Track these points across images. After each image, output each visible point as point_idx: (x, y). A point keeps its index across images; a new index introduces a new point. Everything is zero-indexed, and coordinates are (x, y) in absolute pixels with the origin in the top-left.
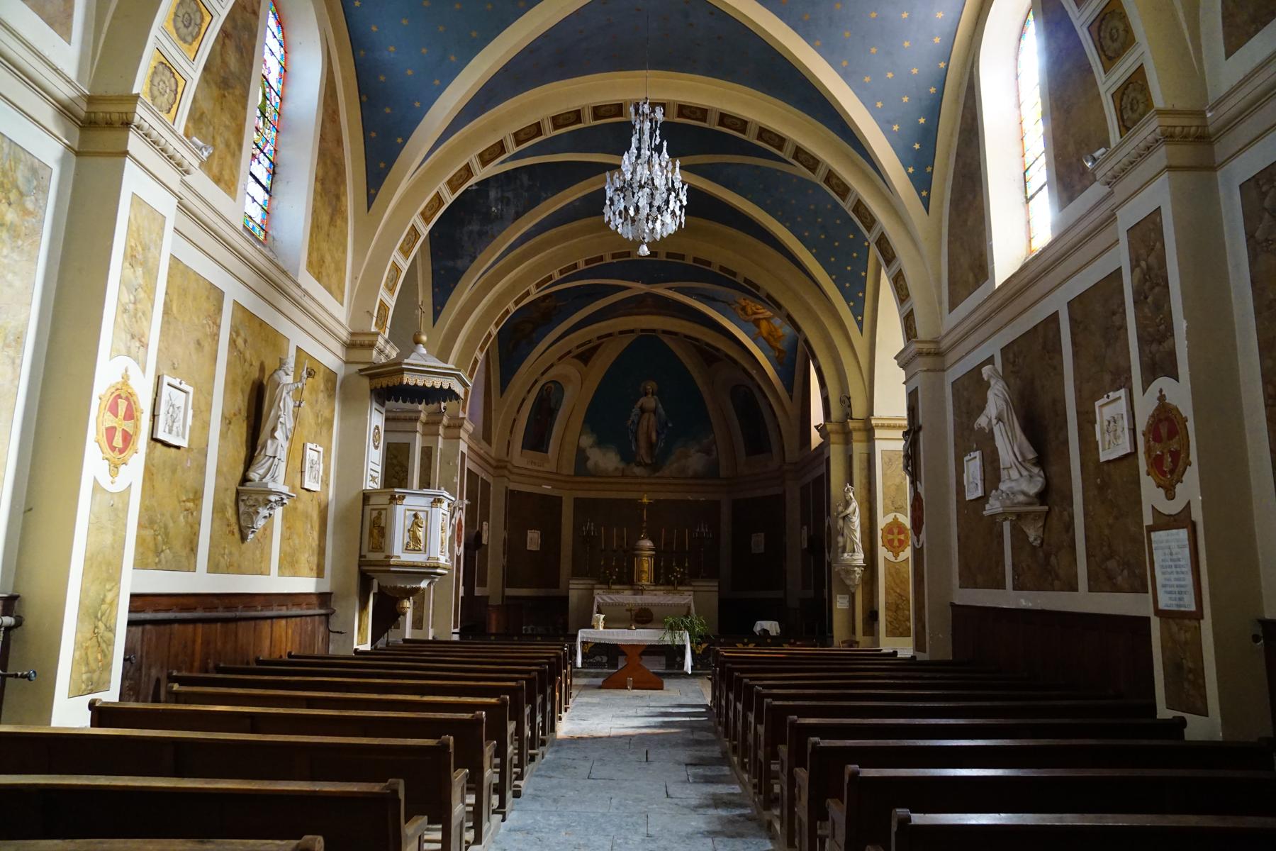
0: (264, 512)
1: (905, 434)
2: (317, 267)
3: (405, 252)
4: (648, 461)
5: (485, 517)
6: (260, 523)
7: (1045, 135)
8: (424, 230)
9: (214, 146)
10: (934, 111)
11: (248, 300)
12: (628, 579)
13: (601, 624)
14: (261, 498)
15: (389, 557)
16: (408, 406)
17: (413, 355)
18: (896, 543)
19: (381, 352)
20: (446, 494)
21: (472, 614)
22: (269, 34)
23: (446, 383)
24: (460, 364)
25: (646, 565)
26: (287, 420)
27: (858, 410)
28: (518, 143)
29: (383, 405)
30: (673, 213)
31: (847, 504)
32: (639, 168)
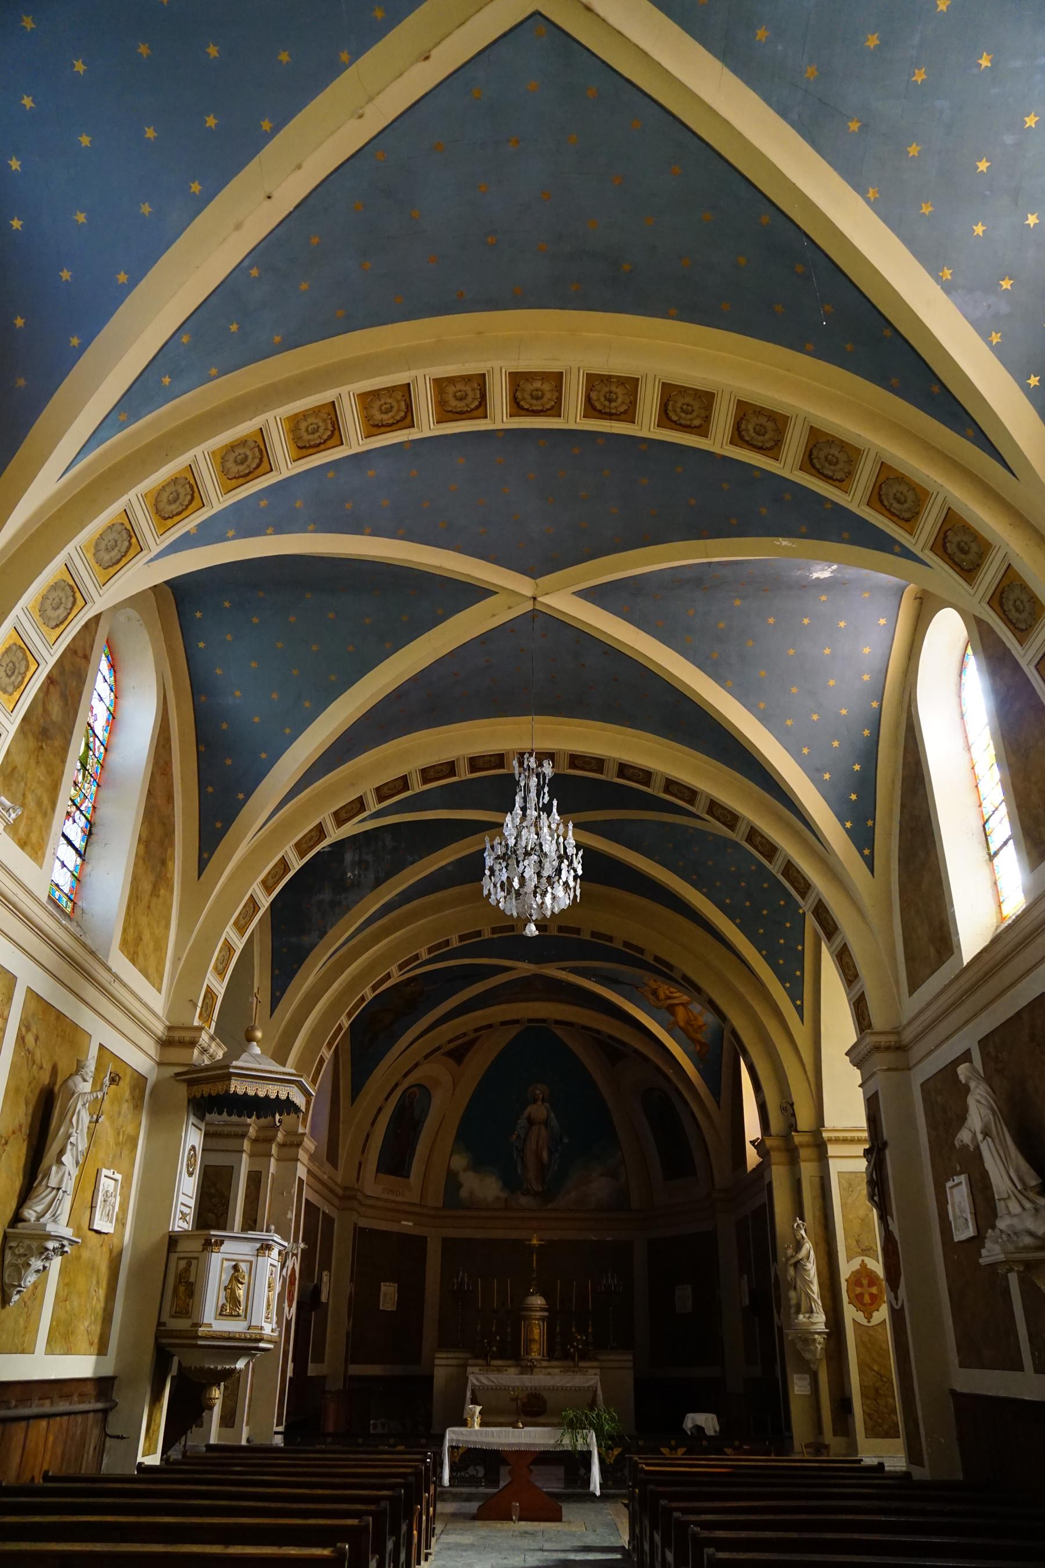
0: (37, 1263)
1: (867, 1153)
2: (132, 948)
3: (241, 928)
4: (538, 1188)
5: (326, 1265)
6: (31, 1279)
7: (1002, 781)
8: (265, 902)
9: (23, 805)
10: (869, 754)
11: (45, 987)
12: (512, 1351)
13: (477, 1420)
14: (35, 1245)
15: (198, 1325)
16: (234, 1118)
17: (244, 1056)
18: (867, 1299)
19: (204, 1051)
20: (277, 1238)
21: (303, 1400)
22: (100, 677)
23: (283, 1092)
24: (302, 1066)
25: (537, 1331)
26: (79, 1139)
27: (804, 1120)
28: (381, 798)
29: (201, 1117)
30: (566, 883)
31: (799, 1245)
32: (524, 832)
